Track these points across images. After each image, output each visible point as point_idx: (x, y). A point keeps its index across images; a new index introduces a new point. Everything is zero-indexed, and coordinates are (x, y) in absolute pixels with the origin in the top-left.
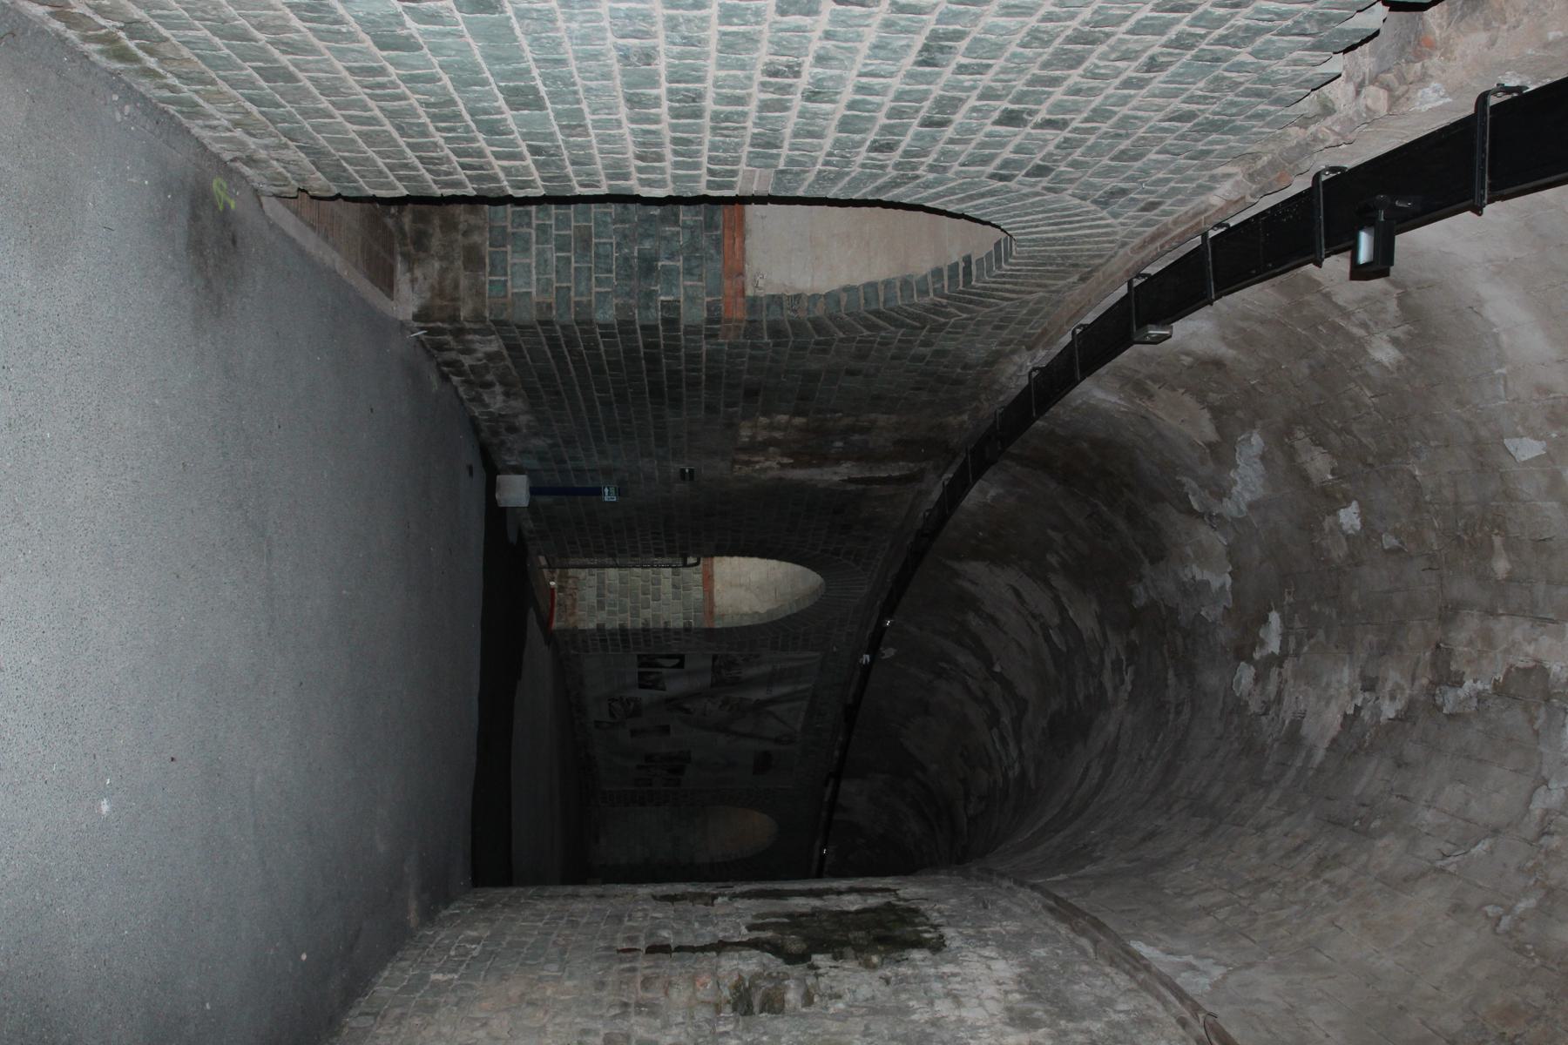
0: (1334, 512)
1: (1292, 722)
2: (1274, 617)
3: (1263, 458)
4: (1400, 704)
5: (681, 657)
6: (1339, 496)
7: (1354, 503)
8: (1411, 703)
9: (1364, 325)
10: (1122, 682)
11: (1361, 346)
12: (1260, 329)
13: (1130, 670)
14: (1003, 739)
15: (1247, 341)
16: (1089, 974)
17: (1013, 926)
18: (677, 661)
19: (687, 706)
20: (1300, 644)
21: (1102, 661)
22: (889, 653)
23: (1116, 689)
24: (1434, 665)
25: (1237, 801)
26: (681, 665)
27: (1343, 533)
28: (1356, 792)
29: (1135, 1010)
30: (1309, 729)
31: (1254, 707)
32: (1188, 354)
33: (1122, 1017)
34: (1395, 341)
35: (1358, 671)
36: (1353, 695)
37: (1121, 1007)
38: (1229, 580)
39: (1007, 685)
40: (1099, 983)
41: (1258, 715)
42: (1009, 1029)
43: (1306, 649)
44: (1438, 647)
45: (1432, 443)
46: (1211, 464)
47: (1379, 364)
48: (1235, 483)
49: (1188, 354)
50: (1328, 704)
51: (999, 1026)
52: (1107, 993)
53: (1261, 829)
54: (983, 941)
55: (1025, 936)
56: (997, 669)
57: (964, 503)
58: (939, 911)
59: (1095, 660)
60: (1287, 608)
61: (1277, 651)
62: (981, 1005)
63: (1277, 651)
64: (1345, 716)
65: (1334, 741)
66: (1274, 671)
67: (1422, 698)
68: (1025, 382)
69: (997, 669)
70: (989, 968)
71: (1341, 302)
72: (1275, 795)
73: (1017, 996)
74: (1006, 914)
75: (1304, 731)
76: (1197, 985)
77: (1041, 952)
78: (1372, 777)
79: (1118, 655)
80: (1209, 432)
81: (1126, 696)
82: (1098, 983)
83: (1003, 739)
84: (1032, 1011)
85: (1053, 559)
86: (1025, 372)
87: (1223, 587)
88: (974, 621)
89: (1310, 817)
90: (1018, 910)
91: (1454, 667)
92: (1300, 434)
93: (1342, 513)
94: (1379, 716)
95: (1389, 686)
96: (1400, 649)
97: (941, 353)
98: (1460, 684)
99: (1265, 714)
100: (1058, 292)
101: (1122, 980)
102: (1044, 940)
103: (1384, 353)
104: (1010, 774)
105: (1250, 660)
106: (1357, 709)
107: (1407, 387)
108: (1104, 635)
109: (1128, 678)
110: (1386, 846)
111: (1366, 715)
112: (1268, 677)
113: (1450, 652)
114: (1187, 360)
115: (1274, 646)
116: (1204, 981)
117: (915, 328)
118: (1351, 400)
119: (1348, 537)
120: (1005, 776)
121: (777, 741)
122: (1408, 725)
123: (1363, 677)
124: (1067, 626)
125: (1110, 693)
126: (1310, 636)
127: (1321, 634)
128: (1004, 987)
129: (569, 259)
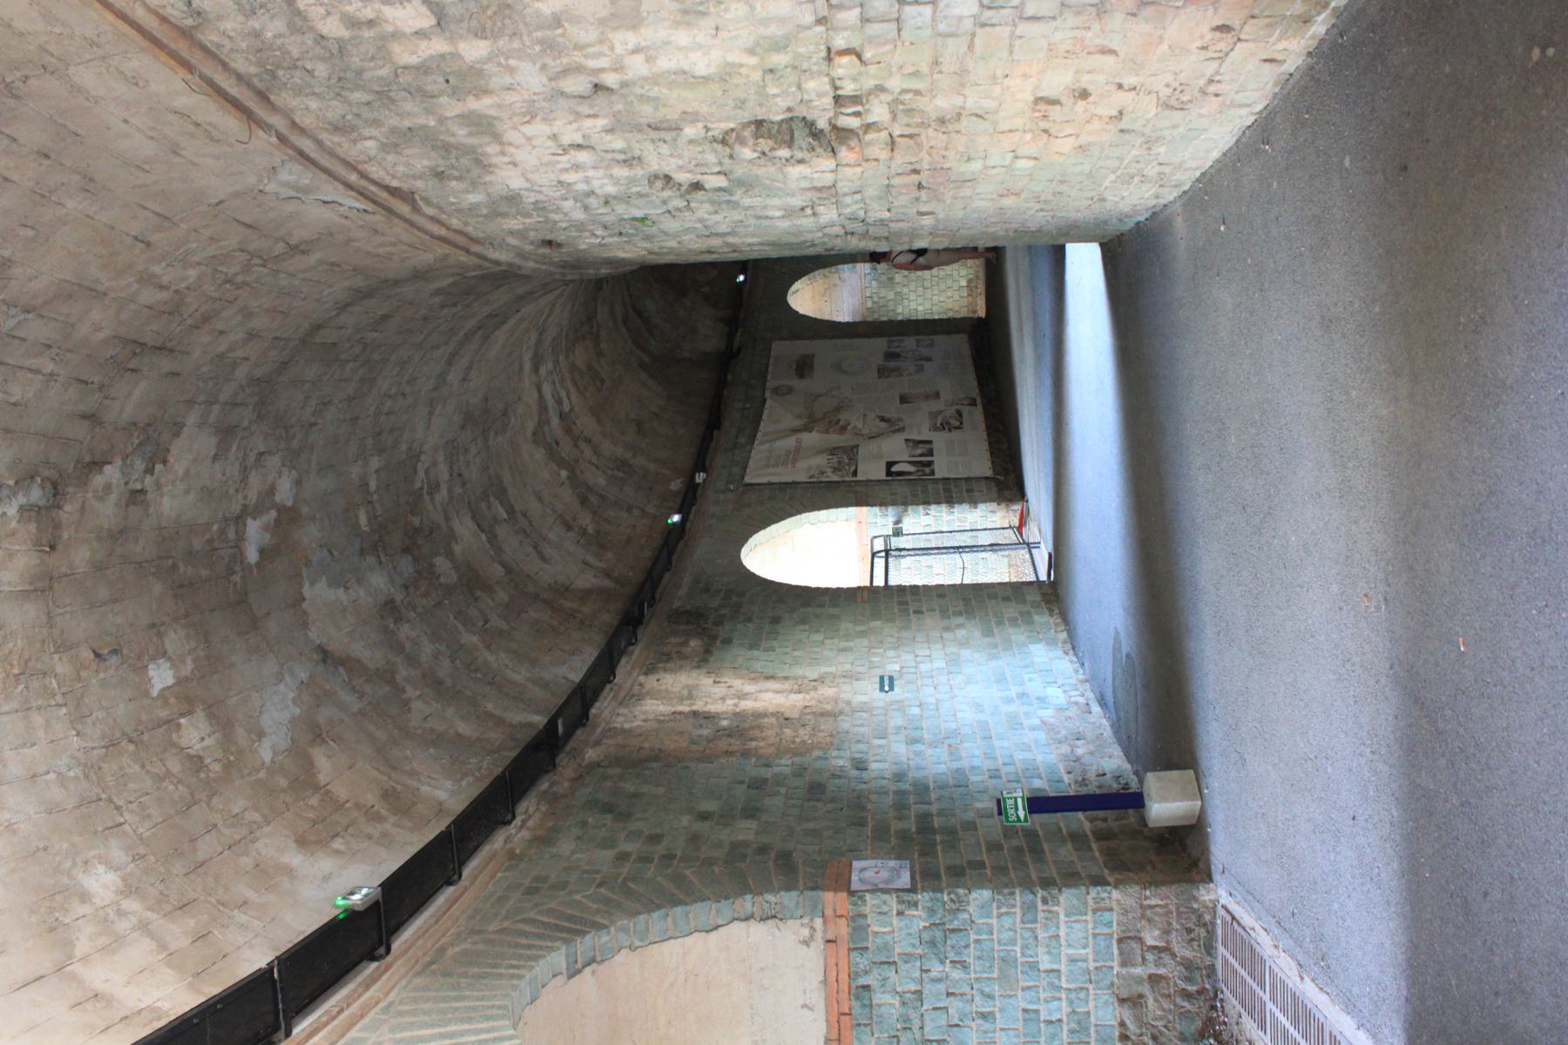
0: (180, 681)
1: (228, 450)
2: (252, 556)
3: (261, 734)
4: (98, 481)
5: (889, 473)
6: (172, 700)
7: (155, 693)
8: (83, 482)
9: (121, 914)
10: (427, 472)
11: (130, 889)
12: (250, 894)
13: (418, 485)
14: (559, 402)
15: (267, 875)
16: (415, 177)
17: (514, 224)
18: (894, 469)
19: (883, 425)
20: (222, 531)
21: (450, 491)
22: (676, 485)
23: (435, 464)
24: (57, 526)
25: (285, 363)
26: (890, 464)
27: (169, 659)
28: (143, 385)
29: (354, 142)
30: (206, 443)
31: (274, 461)
32: (338, 852)
33: (366, 132)
34: (85, 897)
35: (152, 510)
36: (158, 485)
37: (370, 144)
38: (306, 591)
39: (553, 454)
40: (401, 169)
41: (270, 453)
42: (492, 112)
43: (215, 527)
44: (52, 547)
45: (52, 776)
46: (321, 720)
47: (111, 866)
48: (294, 702)
49: (338, 852)
50: (187, 473)
51: (505, 115)
52: (391, 158)
53: (252, 335)
54: (539, 207)
55: (496, 214)
56: (564, 473)
57: (595, 654)
58: (596, 236)
59: (458, 490)
60: (237, 568)
61: (250, 521)
62: (529, 139)
63: (250, 521)
64: (165, 462)
65: (177, 434)
66: (253, 496)
67: (70, 489)
68: (522, 807)
69: (564, 473)
70: (527, 180)
71: (147, 940)
72: (241, 373)
73: (489, 150)
74: (521, 234)
75: (214, 440)
76: (294, 173)
77: (473, 198)
78: (132, 400)
79: (432, 499)
80: (324, 764)
81: (423, 458)
82: (408, 167)
83: (559, 402)
84: (471, 134)
85: (502, 596)
86: (518, 821)
87: (312, 584)
88: (586, 521)
89: (197, 353)
90: (512, 241)
91: (32, 527)
92: (217, 767)
93: (170, 681)
94: (124, 464)
95: (113, 497)
96: (100, 539)
97: (607, 843)
98: (22, 509)
99: (261, 454)
100: (473, 932)
101: (375, 171)
102: (473, 209)
103: (101, 882)
104: (550, 365)
105: (282, 509)
106: (150, 471)
107: (76, 839)
108: (447, 519)
109: (421, 474)
110: (100, 330)
111: (140, 465)
112: (260, 494)
113: (38, 543)
114: (338, 844)
115: (253, 527)
116: (284, 176)
117: (634, 880)
118: (149, 816)
119: (164, 654)
120: (556, 362)
121: (790, 390)
122: (87, 459)
123: (145, 504)
124: (487, 527)
125: (441, 458)
126: (210, 541)
127: (197, 544)
128: (506, 159)
129: (1023, 955)
